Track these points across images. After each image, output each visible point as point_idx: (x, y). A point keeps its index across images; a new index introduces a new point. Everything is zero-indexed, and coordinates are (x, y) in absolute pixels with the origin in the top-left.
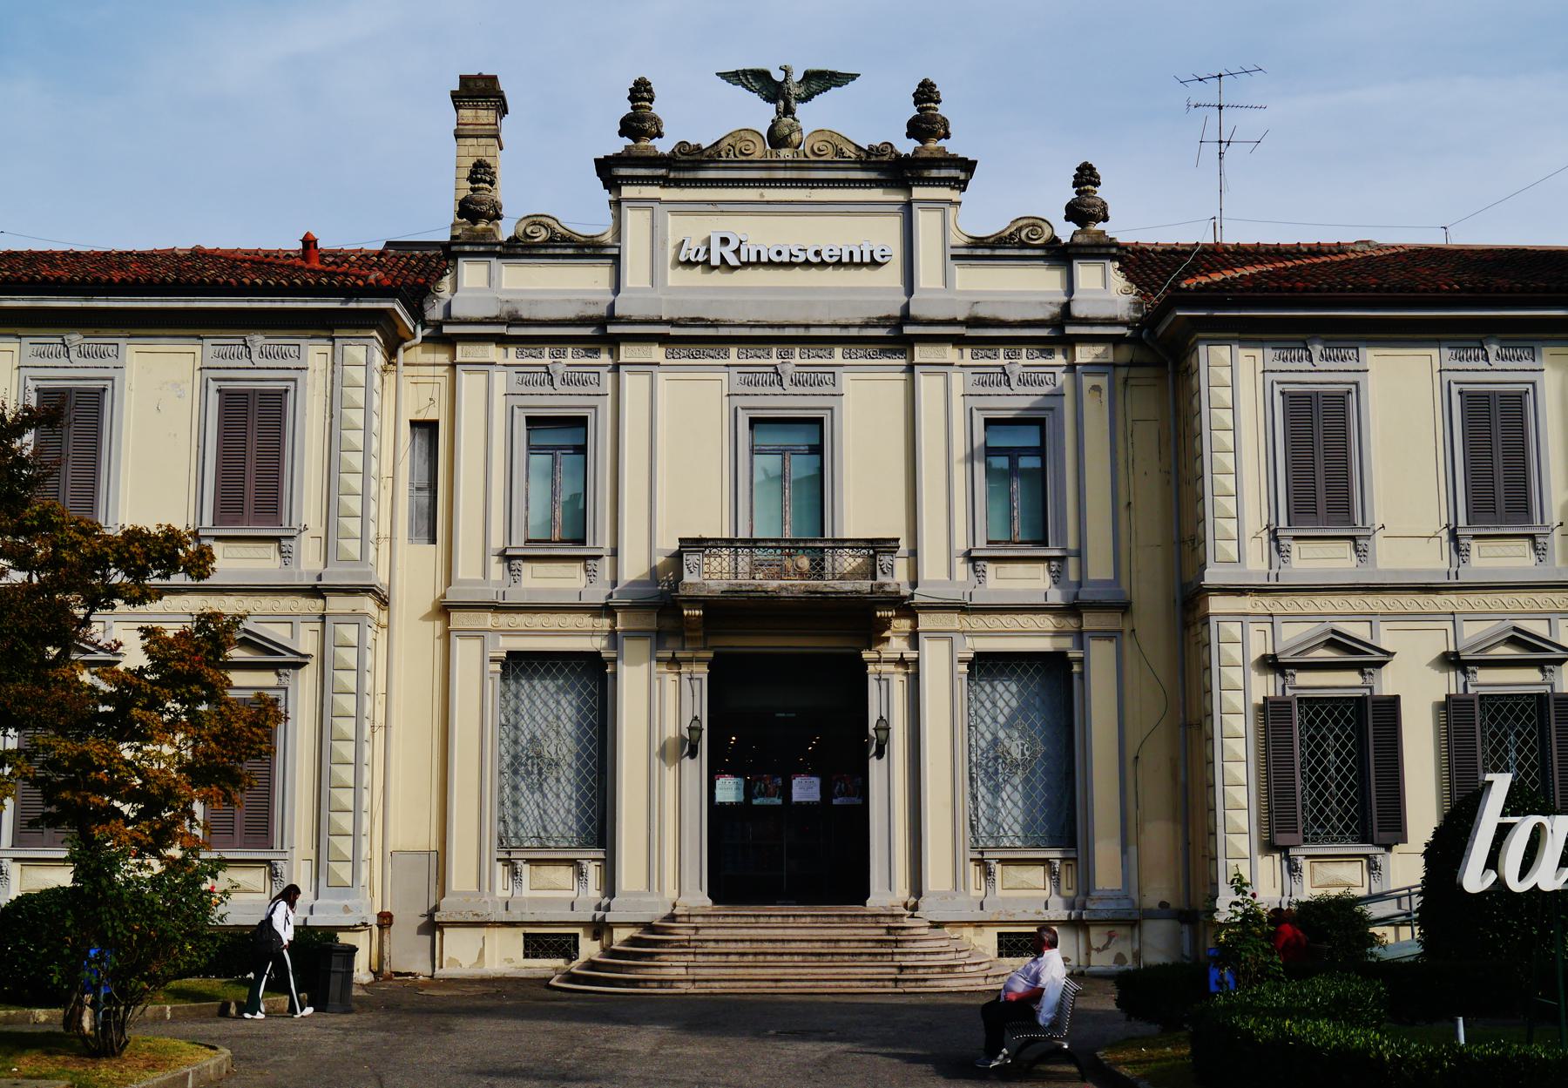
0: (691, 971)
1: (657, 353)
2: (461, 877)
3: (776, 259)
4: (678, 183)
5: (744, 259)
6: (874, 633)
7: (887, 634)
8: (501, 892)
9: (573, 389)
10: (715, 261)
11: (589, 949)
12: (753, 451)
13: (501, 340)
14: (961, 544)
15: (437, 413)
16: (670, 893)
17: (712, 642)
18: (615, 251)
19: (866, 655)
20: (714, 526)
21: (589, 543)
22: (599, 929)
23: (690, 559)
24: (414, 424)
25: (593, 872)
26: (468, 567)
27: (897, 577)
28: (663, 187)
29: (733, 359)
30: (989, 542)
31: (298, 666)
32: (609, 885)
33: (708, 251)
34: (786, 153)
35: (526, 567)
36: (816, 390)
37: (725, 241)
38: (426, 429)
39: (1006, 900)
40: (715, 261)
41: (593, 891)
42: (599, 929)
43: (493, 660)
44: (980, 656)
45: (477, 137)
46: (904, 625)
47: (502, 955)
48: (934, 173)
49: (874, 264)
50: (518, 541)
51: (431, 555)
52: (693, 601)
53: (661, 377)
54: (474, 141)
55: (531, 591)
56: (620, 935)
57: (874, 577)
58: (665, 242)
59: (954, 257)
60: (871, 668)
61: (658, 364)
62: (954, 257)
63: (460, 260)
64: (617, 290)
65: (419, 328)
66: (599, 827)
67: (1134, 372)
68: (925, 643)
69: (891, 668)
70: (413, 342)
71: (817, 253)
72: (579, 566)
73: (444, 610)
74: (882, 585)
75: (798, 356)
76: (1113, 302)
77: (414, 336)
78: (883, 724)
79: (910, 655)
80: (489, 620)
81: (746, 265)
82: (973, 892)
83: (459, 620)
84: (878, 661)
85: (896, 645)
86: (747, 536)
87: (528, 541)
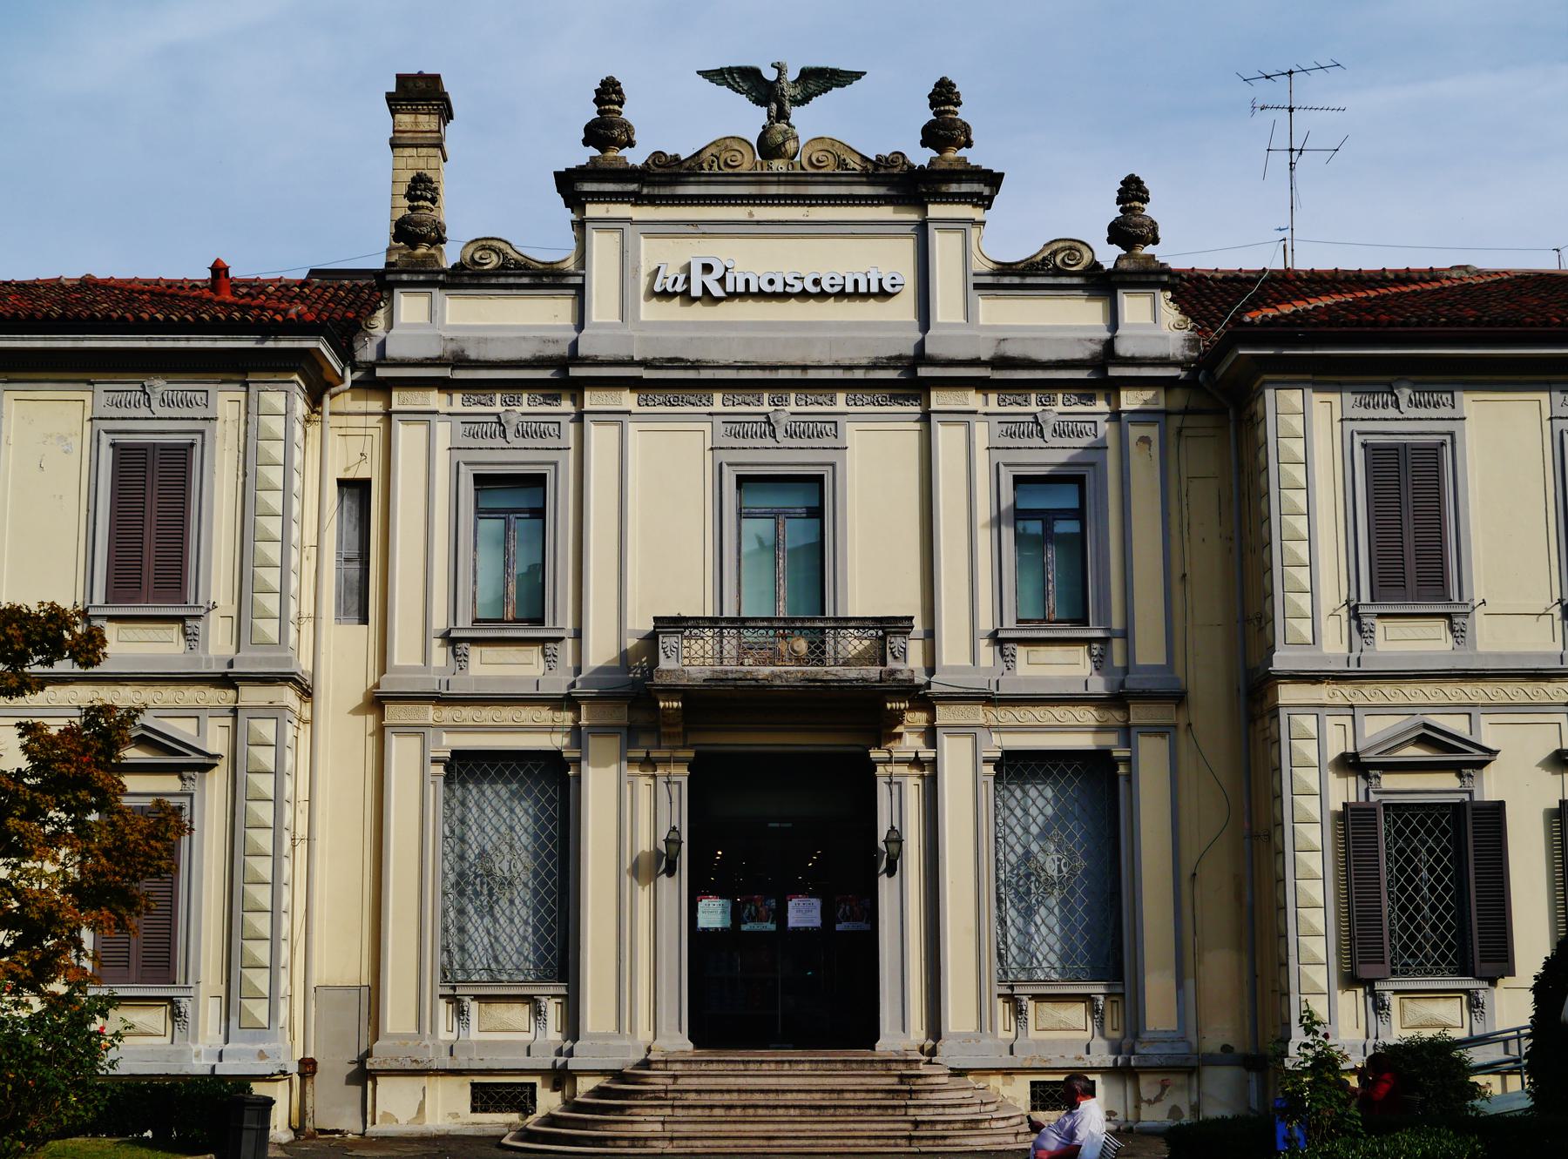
0: (668, 1127)
1: (628, 400)
2: (398, 1016)
3: (767, 288)
4: (653, 201)
5: (730, 288)
6: (885, 729)
7: (899, 729)
8: (444, 1035)
9: (529, 442)
10: (696, 291)
11: (548, 1101)
12: (741, 515)
13: (445, 385)
14: (986, 624)
15: (369, 470)
16: (644, 1034)
17: (694, 739)
18: (578, 280)
19: (875, 754)
20: (695, 601)
21: (549, 622)
22: (560, 1077)
23: (667, 641)
24: (342, 483)
25: (552, 1010)
26: (405, 652)
27: (913, 661)
28: (635, 204)
29: (718, 406)
30: (1018, 621)
31: (205, 768)
32: (572, 1026)
33: (688, 280)
34: (778, 165)
35: (475, 652)
36: (815, 442)
37: (707, 268)
38: (355, 489)
39: (1040, 1044)
40: (696, 291)
41: (552, 1032)
42: (560, 1077)
43: (435, 761)
44: (457, 754)
45: (416, 146)
46: (920, 718)
47: (446, 1109)
48: (954, 188)
49: (883, 295)
50: (464, 620)
51: (361, 638)
52: (671, 691)
53: (632, 428)
54: (413, 151)
55: (479, 680)
56: (585, 1085)
57: (884, 663)
58: (637, 270)
59: (977, 286)
60: (880, 769)
61: (629, 413)
62: (977, 286)
63: (397, 291)
64: (580, 325)
65: (348, 372)
66: (559, 957)
67: (1190, 421)
68: (945, 741)
69: (904, 769)
70: (342, 387)
71: (816, 282)
72: (536, 651)
73: (377, 702)
74: (893, 672)
75: (793, 404)
76: (1164, 338)
77: (342, 380)
78: (895, 836)
79: (927, 754)
80: (430, 713)
81: (732, 296)
82: (1002, 1034)
83: (394, 714)
84: (889, 761)
85: (910, 743)
86: (734, 615)
87: (476, 621)
